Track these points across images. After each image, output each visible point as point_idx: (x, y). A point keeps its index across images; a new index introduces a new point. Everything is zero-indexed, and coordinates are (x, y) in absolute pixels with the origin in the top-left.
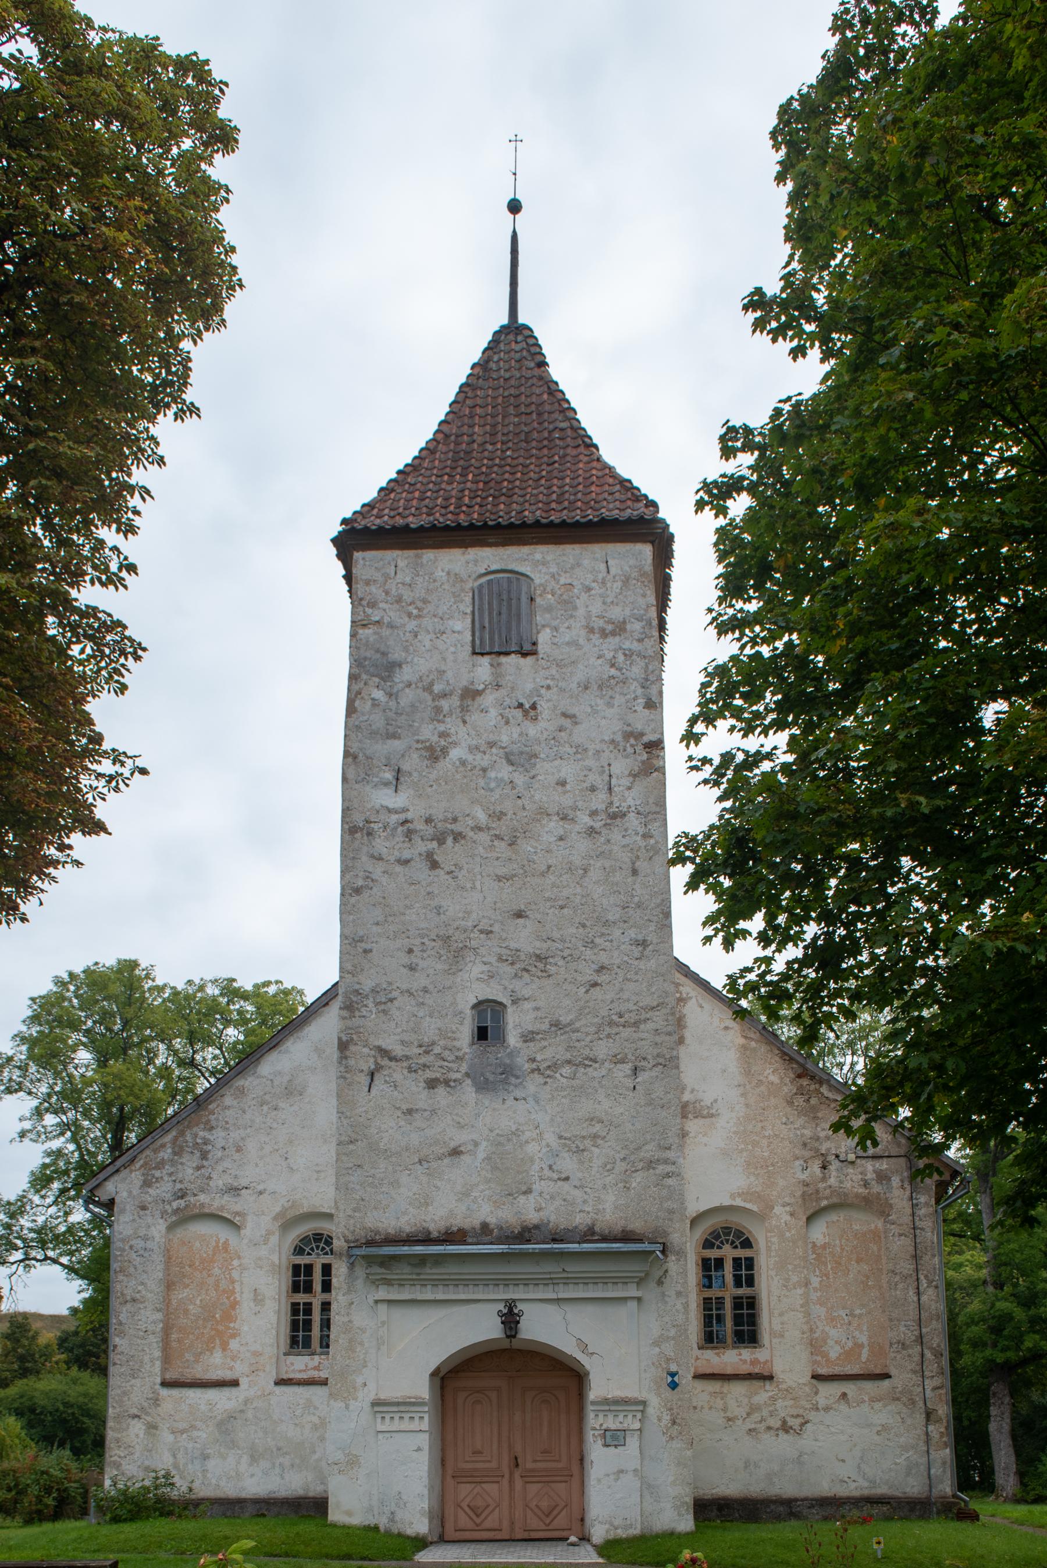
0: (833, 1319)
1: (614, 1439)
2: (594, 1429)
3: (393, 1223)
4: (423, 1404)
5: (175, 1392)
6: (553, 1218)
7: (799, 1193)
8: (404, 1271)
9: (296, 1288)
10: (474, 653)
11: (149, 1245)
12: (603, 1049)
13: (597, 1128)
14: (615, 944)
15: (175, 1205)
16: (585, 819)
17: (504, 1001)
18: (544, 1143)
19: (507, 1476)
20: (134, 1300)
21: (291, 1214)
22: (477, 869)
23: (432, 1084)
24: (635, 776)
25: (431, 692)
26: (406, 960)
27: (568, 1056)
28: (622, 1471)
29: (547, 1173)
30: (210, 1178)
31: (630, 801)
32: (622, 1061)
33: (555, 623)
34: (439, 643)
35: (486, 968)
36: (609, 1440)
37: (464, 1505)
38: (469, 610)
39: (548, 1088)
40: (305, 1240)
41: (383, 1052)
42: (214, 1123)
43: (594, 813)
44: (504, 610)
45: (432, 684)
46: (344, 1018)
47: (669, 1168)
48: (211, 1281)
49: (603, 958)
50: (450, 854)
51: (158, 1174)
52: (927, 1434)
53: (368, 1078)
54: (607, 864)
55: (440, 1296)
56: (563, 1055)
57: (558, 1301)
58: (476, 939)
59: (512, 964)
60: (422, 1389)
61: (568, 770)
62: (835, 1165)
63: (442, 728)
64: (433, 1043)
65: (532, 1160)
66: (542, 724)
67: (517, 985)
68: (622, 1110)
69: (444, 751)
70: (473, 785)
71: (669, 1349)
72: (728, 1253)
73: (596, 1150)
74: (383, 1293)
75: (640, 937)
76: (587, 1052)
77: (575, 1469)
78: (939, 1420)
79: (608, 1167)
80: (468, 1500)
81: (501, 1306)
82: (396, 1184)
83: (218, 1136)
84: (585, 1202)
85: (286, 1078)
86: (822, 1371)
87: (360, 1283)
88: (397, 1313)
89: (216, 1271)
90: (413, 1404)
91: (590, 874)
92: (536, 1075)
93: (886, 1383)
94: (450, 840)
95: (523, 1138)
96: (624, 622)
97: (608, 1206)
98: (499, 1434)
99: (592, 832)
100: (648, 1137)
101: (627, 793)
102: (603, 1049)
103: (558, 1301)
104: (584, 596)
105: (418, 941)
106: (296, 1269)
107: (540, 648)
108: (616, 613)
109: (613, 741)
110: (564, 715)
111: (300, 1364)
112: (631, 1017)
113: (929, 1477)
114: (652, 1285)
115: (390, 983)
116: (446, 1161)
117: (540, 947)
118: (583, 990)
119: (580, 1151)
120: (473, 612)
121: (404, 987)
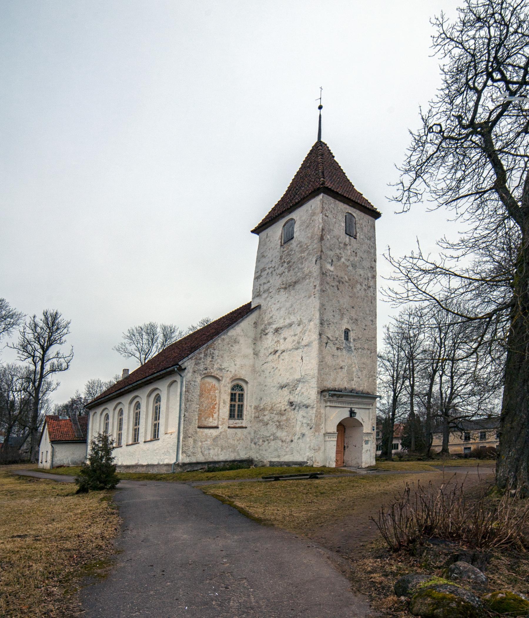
5: (201, 430)
11: (196, 384)
13: (364, 366)
15: (204, 372)
23: (338, 349)
48: (210, 396)
50: (341, 286)
60: (335, 430)
72: (238, 392)
74: (329, 404)
82: (330, 375)
83: (216, 352)
85: (235, 337)
87: (322, 401)
89: (212, 393)
111: (232, 422)
119: (362, 371)
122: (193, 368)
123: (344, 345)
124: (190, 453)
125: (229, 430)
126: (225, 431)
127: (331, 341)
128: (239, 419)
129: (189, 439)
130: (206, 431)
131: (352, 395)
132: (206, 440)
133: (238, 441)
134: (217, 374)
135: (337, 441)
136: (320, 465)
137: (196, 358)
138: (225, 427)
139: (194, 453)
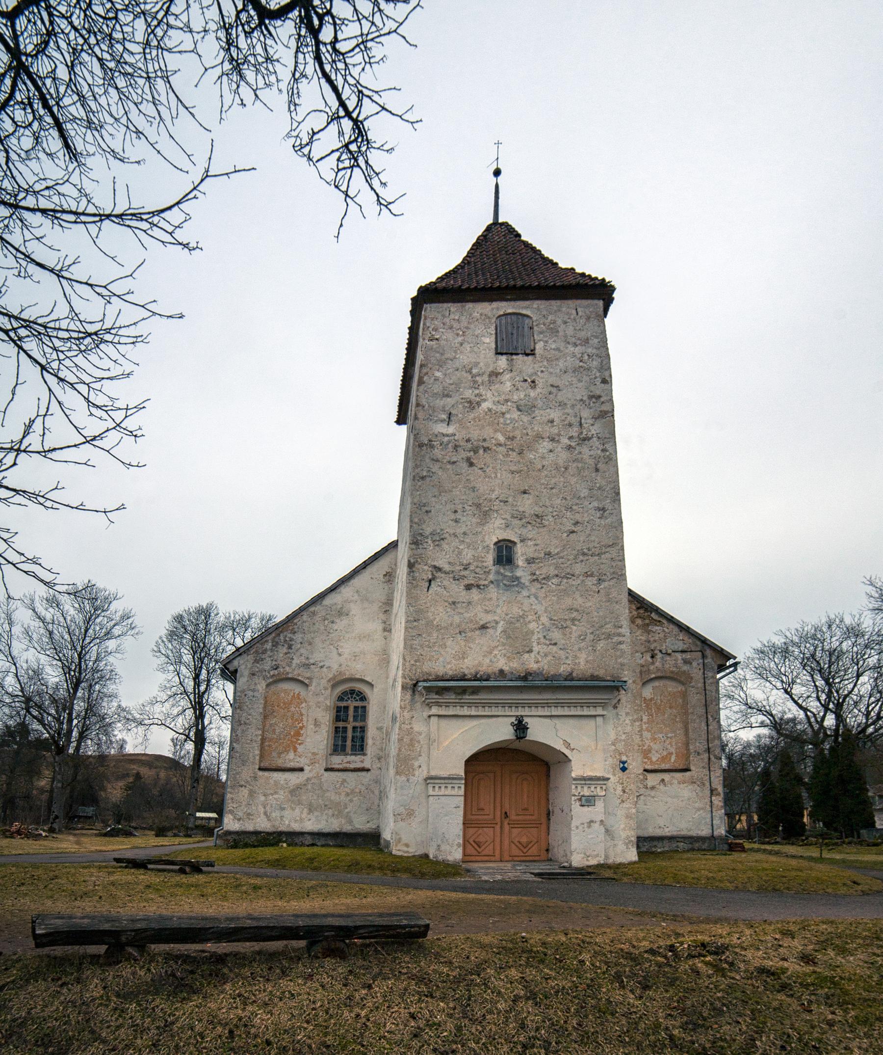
0: (655, 739)
1: (588, 801)
2: (575, 795)
3: (441, 669)
4: (460, 779)
5: (266, 774)
6: (546, 667)
7: (638, 671)
8: (451, 697)
9: (338, 719)
10: (497, 353)
11: (256, 694)
12: (578, 569)
13: (575, 614)
14: (585, 509)
15: (272, 673)
16: (565, 441)
17: (515, 540)
18: (540, 623)
19: (499, 824)
20: (245, 724)
21: (339, 678)
22: (499, 467)
23: (468, 587)
24: (596, 419)
25: (471, 373)
26: (453, 517)
27: (556, 572)
28: (592, 821)
29: (542, 640)
30: (293, 659)
31: (593, 432)
32: (592, 575)
33: (545, 339)
34: (476, 349)
35: (503, 521)
36: (584, 802)
37: (471, 841)
38: (494, 332)
39: (543, 590)
40: (345, 693)
41: (438, 569)
42: (296, 630)
43: (571, 438)
44: (515, 332)
45: (471, 369)
46: (412, 549)
47: (621, 639)
49: (578, 517)
50: (481, 458)
51: (263, 657)
52: (711, 802)
53: (427, 584)
54: (580, 465)
55: (473, 713)
56: (552, 571)
57: (551, 716)
58: (497, 505)
59: (521, 519)
60: (460, 770)
61: (555, 414)
62: (659, 655)
63: (477, 392)
64: (469, 564)
65: (533, 633)
66: (538, 390)
67: (524, 531)
68: (590, 604)
69: (479, 404)
70: (496, 421)
71: (620, 746)
73: (574, 628)
74: (435, 710)
75: (601, 506)
76: (568, 570)
77: (544, 820)
78: (719, 794)
79: (582, 638)
80: (473, 838)
81: (513, 720)
82: (444, 646)
83: (298, 637)
84: (567, 658)
85: (339, 607)
86: (649, 767)
87: (418, 705)
88: (444, 722)
89: (293, 709)
90: (455, 779)
91: (570, 470)
92: (536, 583)
93: (688, 774)
94: (481, 451)
95: (527, 620)
96: (587, 339)
97: (582, 661)
98: (495, 800)
99: (569, 447)
100: (608, 620)
101: (591, 428)
102: (578, 569)
103: (551, 716)
104: (563, 326)
105: (461, 506)
106: (338, 709)
107: (536, 351)
108: (583, 335)
109: (582, 400)
110: (552, 386)
111: (337, 761)
112: (597, 551)
113: (712, 825)
114: (611, 708)
115: (442, 530)
116: (477, 632)
117: (538, 510)
118: (565, 535)
120: (496, 334)
121: (452, 532)
122: (252, 668)
123: (491, 577)
124: (240, 814)
125: (326, 774)
126: (319, 777)
127: (446, 573)
128: (355, 755)
129: (241, 789)
130: (276, 775)
131: (570, 687)
132: (276, 793)
133: (347, 794)
134: (299, 675)
135: (465, 796)
136: (414, 850)
137: (256, 652)
138: (319, 768)
139: (249, 814)
